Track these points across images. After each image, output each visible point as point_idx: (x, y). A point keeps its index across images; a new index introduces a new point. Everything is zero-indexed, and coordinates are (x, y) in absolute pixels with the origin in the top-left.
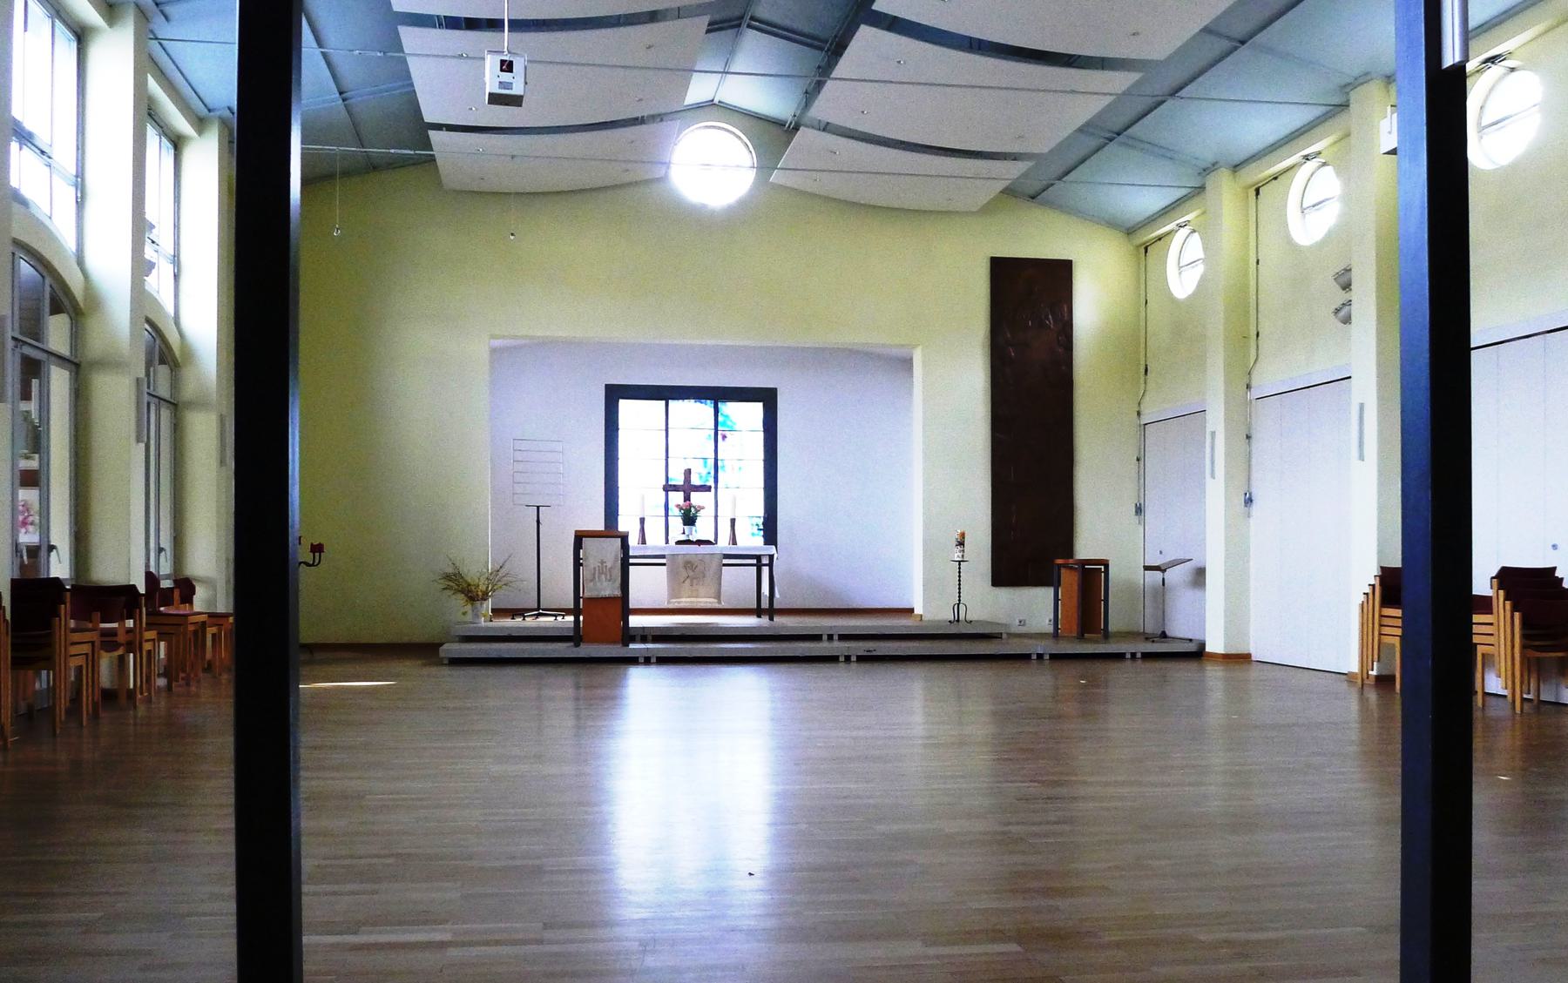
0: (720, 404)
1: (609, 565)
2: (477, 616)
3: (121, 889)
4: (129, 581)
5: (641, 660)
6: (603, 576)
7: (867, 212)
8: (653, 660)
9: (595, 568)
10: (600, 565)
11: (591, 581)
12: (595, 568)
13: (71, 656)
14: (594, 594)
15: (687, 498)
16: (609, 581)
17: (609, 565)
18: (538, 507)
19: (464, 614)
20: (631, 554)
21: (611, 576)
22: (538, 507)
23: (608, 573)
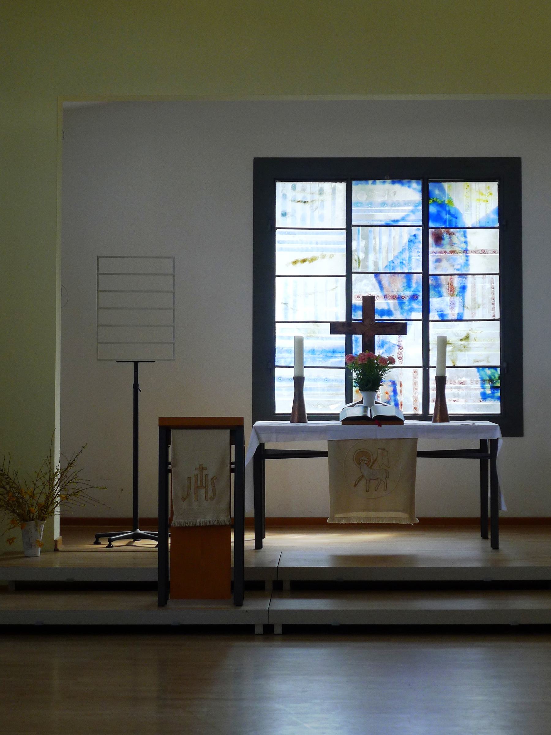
0: (431, 186)
1: (211, 472)
2: (30, 545)
3: (330, 395)
4: (293, 357)
5: (259, 630)
6: (202, 492)
7: (443, 292)
8: (278, 630)
9: (189, 479)
10: (197, 472)
11: (184, 499)
12: (189, 479)
13: (305, 367)
14: (189, 521)
15: (369, 345)
16: (212, 499)
17: (211, 472)
18: (136, 364)
19: (11, 541)
20: (498, 276)
21: (214, 491)
22: (136, 364)
23: (210, 486)
